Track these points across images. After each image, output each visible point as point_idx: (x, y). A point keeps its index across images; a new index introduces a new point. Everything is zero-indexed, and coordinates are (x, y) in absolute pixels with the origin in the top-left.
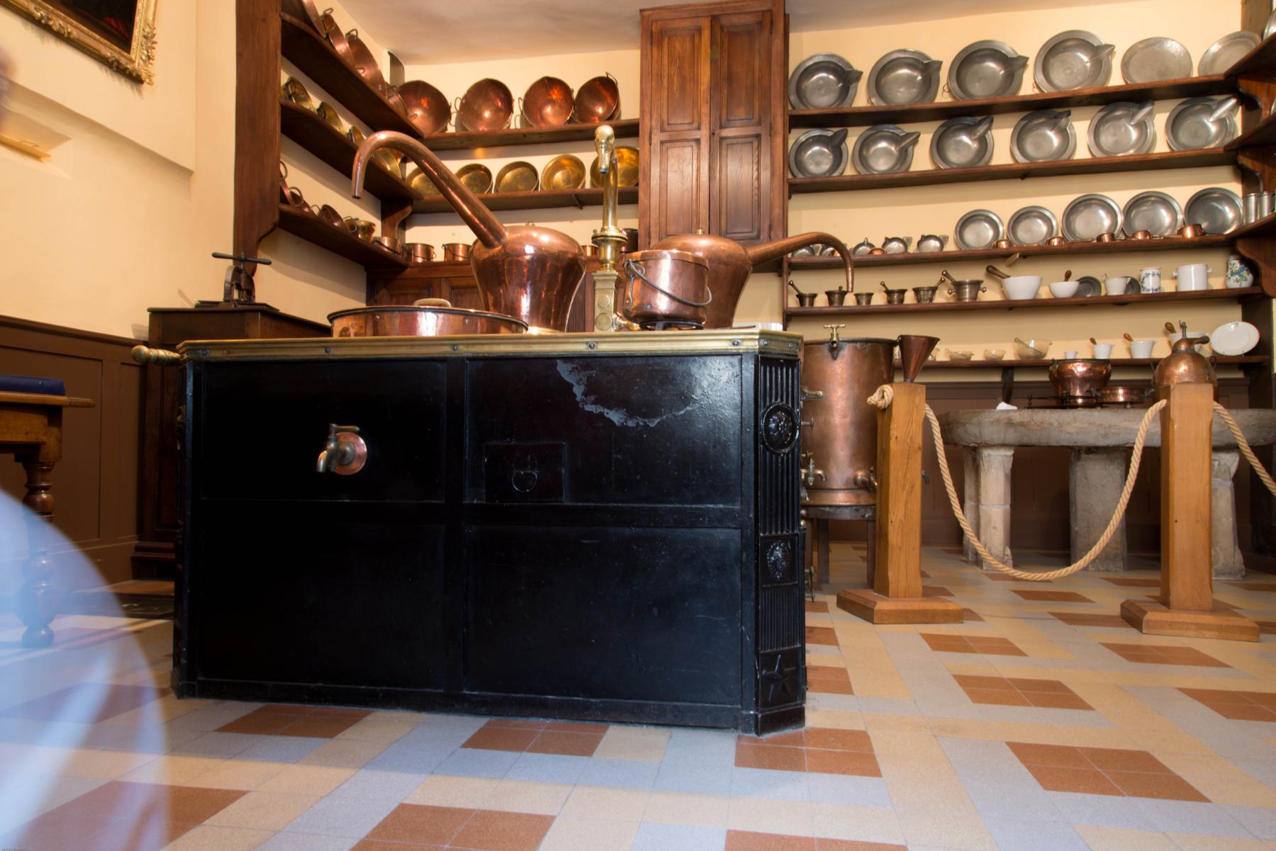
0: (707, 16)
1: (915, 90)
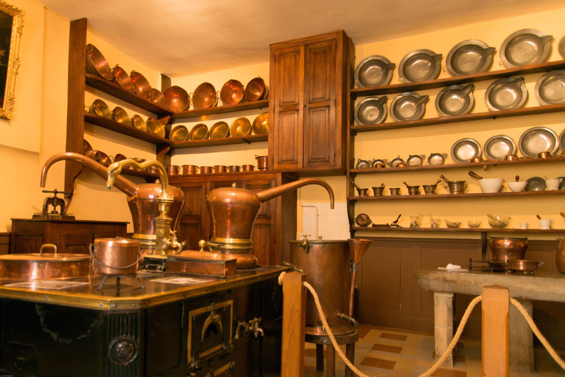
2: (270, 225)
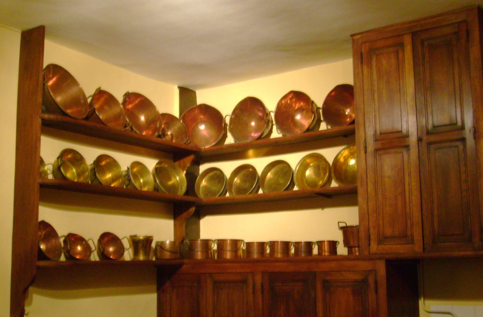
0: (409, 33)
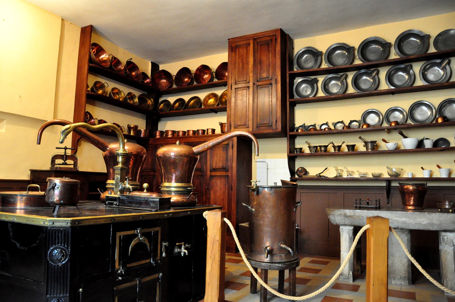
1: (345, 59)
2: (228, 176)
